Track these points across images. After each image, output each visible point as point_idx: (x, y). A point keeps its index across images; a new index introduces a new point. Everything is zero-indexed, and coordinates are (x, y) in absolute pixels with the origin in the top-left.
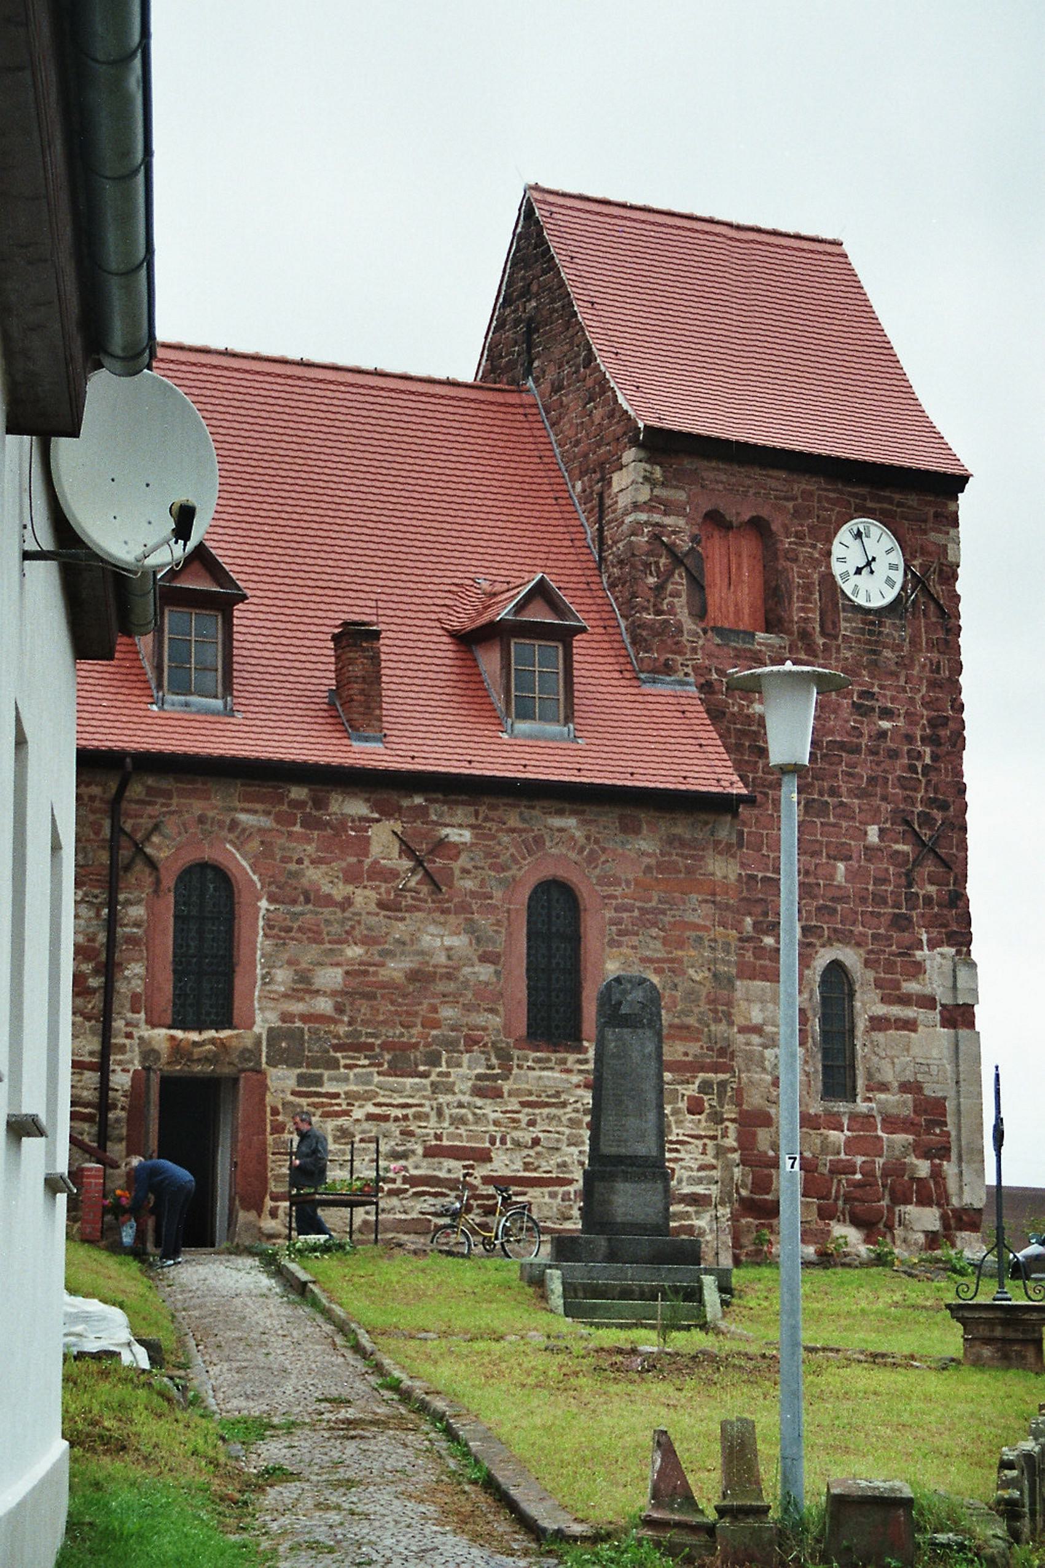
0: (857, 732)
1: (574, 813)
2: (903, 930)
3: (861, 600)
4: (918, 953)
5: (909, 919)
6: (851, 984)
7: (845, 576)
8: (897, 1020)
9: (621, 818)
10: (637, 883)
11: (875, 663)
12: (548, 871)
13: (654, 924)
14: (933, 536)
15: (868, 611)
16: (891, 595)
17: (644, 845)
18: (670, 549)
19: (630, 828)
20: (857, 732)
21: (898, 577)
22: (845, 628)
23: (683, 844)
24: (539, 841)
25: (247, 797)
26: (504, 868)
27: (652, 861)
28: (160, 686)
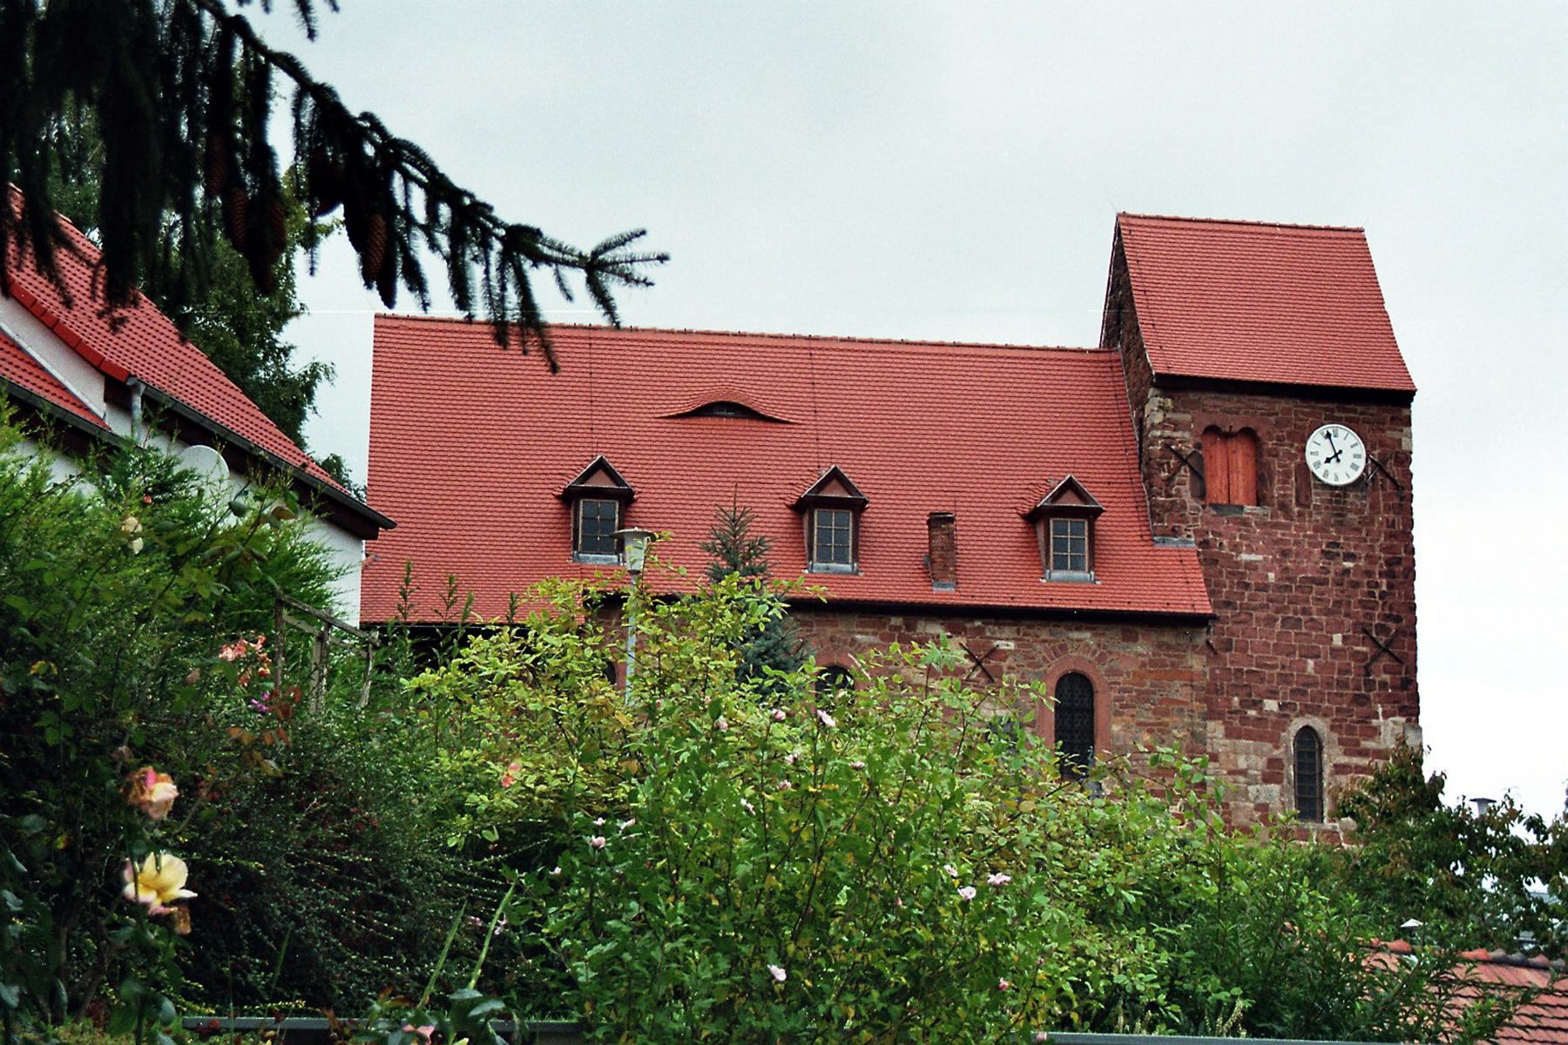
0: (1325, 570)
1: (1087, 629)
2: (1362, 705)
3: (1330, 480)
4: (1374, 722)
5: (1368, 698)
6: (1320, 743)
7: (1317, 464)
8: (1357, 767)
9: (1123, 632)
10: (1135, 673)
11: (1341, 523)
12: (1069, 667)
13: (1147, 701)
14: (1389, 433)
15: (1336, 487)
16: (1355, 475)
17: (1140, 649)
18: (1177, 454)
19: (1131, 638)
20: (1325, 570)
21: (1362, 463)
22: (1315, 500)
23: (1169, 647)
24: (1063, 648)
25: (862, 625)
26: (1038, 666)
27: (1146, 659)
28: (811, 558)
